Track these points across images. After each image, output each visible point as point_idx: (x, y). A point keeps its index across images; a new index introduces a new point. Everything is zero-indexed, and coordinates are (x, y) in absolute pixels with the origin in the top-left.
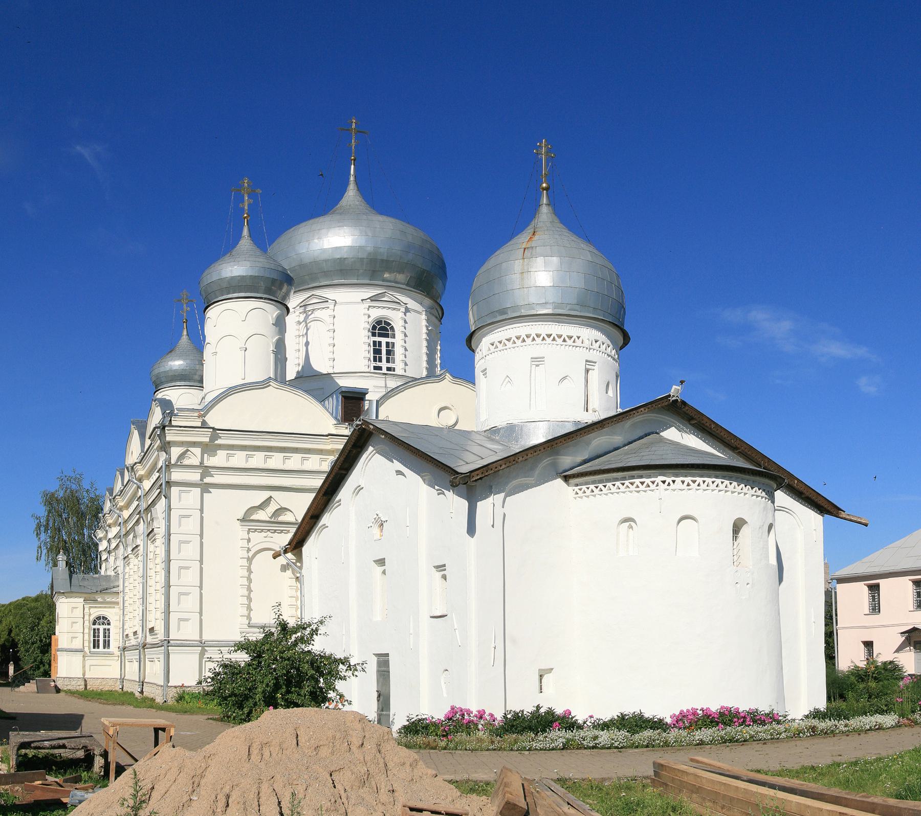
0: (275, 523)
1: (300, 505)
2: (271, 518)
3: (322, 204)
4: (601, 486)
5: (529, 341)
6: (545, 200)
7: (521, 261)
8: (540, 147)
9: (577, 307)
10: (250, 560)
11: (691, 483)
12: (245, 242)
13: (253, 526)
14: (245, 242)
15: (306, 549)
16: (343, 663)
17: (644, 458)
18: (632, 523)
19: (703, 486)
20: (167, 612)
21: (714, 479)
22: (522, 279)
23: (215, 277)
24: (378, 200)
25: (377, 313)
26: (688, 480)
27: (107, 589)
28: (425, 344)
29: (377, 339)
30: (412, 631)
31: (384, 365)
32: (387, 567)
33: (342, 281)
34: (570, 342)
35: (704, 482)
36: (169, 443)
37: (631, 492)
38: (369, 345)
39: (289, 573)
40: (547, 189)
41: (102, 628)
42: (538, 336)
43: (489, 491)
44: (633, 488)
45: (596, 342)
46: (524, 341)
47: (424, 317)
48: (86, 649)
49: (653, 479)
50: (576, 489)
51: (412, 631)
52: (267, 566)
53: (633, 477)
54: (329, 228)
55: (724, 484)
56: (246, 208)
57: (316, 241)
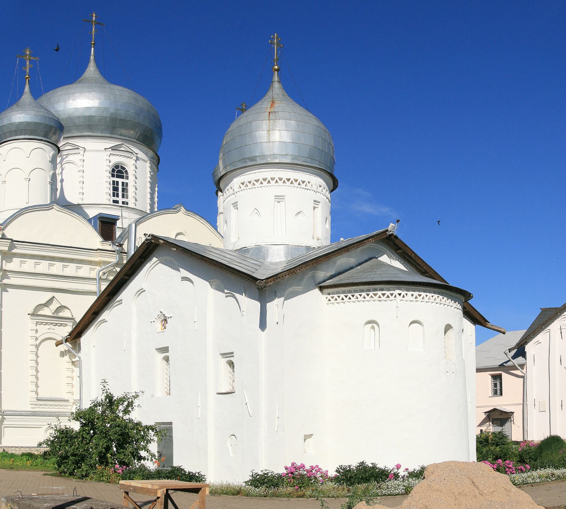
0: (57, 318)
1: (79, 307)
2: (54, 313)
3: (70, 76)
4: (350, 295)
5: (273, 183)
6: (276, 78)
7: (268, 121)
8: (273, 38)
9: (309, 160)
10: (37, 347)
11: (418, 296)
12: (27, 97)
13: (41, 319)
14: (27, 97)
15: (84, 340)
16: (153, 430)
17: (369, 277)
18: (375, 325)
19: (426, 299)
21: (433, 294)
22: (269, 135)
23: (6, 122)
24: (111, 75)
25: (115, 160)
26: (416, 294)
28: (149, 185)
29: (116, 179)
30: (199, 405)
31: (120, 199)
33: (90, 134)
35: (426, 296)
37: (374, 301)
38: (110, 184)
39: (67, 358)
40: (278, 70)
42: (281, 179)
43: (275, 295)
44: (376, 298)
45: (320, 187)
46: (269, 182)
47: (148, 164)
49: (392, 292)
50: (329, 297)
51: (199, 405)
52: (50, 351)
53: (376, 290)
54: (81, 92)
55: (439, 298)
56: (28, 71)
57: (71, 101)
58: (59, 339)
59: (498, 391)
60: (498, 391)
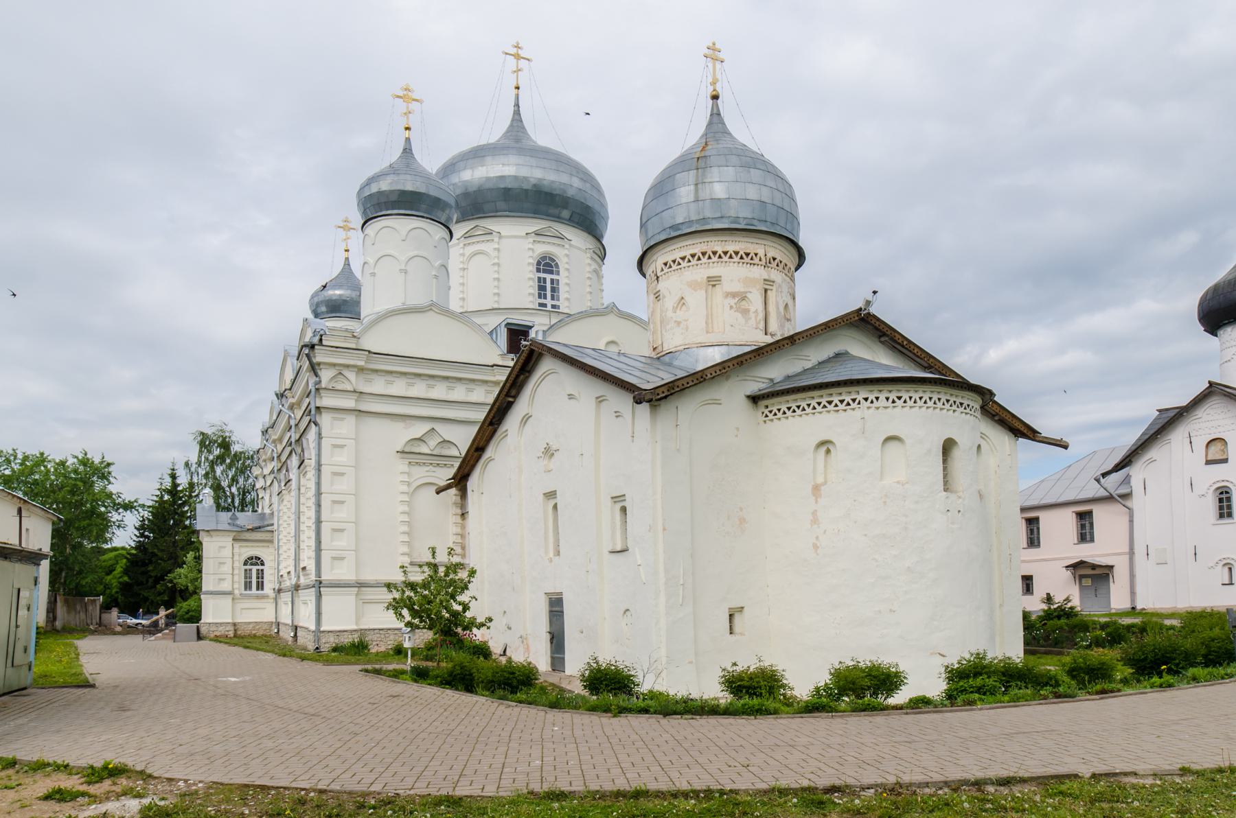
0: (437, 459)
1: (463, 438)
15: (472, 483)
19: (910, 403)
20: (318, 549)
25: (541, 249)
27: (263, 529)
29: (542, 275)
31: (549, 302)
32: (559, 500)
34: (747, 260)
36: (319, 364)
41: (254, 568)
48: (237, 592)
58: (443, 483)
59: (1085, 535)
60: (1085, 535)
